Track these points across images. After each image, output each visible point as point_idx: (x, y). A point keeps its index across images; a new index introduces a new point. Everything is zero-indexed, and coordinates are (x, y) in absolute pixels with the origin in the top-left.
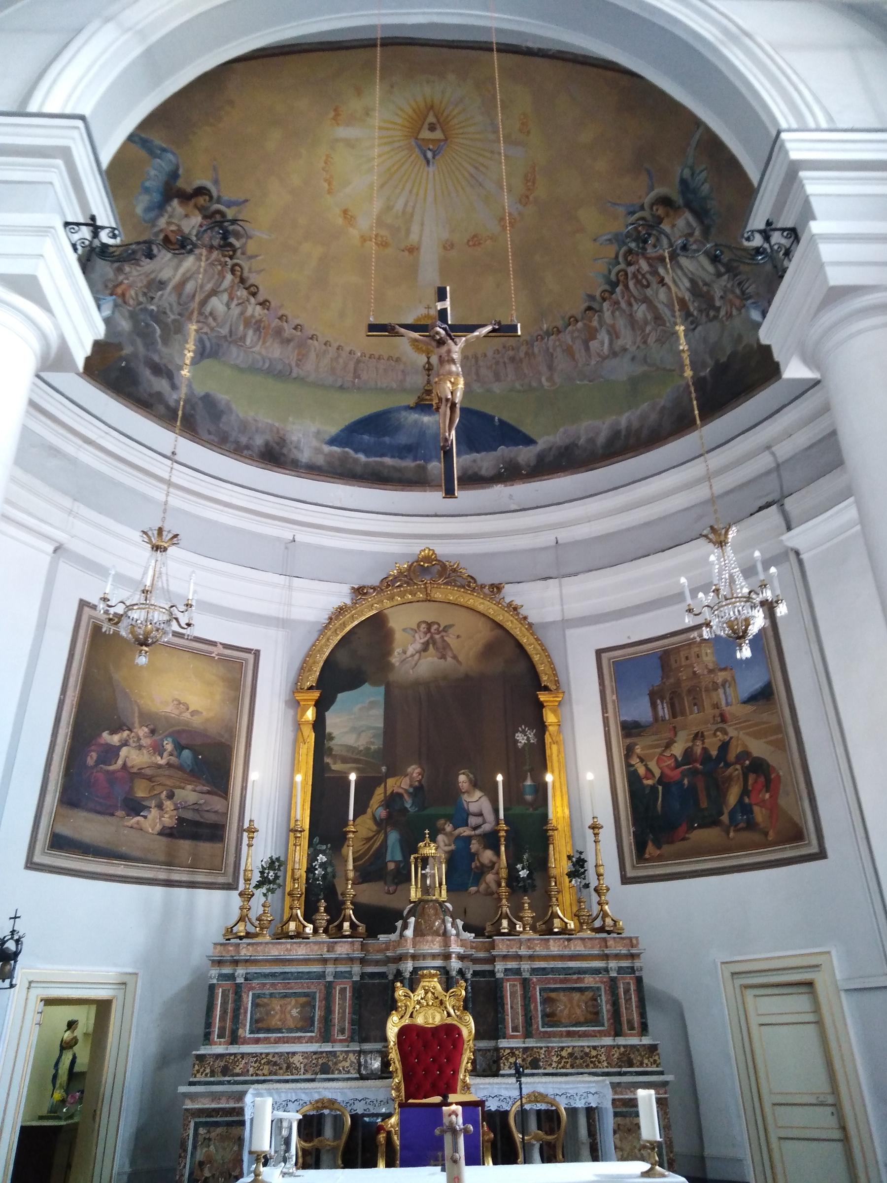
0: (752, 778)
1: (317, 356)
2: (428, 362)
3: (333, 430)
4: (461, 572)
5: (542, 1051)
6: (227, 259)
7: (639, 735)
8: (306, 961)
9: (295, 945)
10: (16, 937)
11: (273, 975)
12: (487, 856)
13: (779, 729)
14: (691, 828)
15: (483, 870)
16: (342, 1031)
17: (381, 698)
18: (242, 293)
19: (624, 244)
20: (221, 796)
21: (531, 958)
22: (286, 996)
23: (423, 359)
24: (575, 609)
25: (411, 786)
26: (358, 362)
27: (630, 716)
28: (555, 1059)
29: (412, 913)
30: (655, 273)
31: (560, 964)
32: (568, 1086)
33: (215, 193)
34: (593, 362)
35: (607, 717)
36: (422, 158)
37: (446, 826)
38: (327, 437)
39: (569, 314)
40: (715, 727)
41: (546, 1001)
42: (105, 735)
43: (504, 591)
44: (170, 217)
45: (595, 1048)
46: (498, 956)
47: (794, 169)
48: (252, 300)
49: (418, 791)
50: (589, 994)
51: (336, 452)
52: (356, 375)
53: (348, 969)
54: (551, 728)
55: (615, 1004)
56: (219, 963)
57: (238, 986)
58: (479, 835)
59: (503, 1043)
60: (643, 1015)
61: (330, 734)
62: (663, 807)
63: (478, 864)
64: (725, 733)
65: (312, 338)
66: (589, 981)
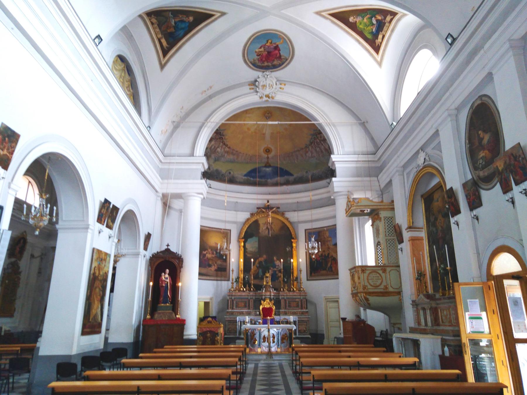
0: (333, 261)
3: (245, 173)
8: (245, 296)
12: (280, 274)
14: (321, 270)
17: (257, 240)
18: (224, 146)
21: (287, 296)
23: (266, 156)
24: (301, 219)
29: (264, 287)
38: (244, 175)
42: (203, 252)
47: (334, 162)
49: (265, 261)
55: (302, 304)
56: (229, 296)
59: (281, 310)
64: (329, 251)
66: (297, 300)
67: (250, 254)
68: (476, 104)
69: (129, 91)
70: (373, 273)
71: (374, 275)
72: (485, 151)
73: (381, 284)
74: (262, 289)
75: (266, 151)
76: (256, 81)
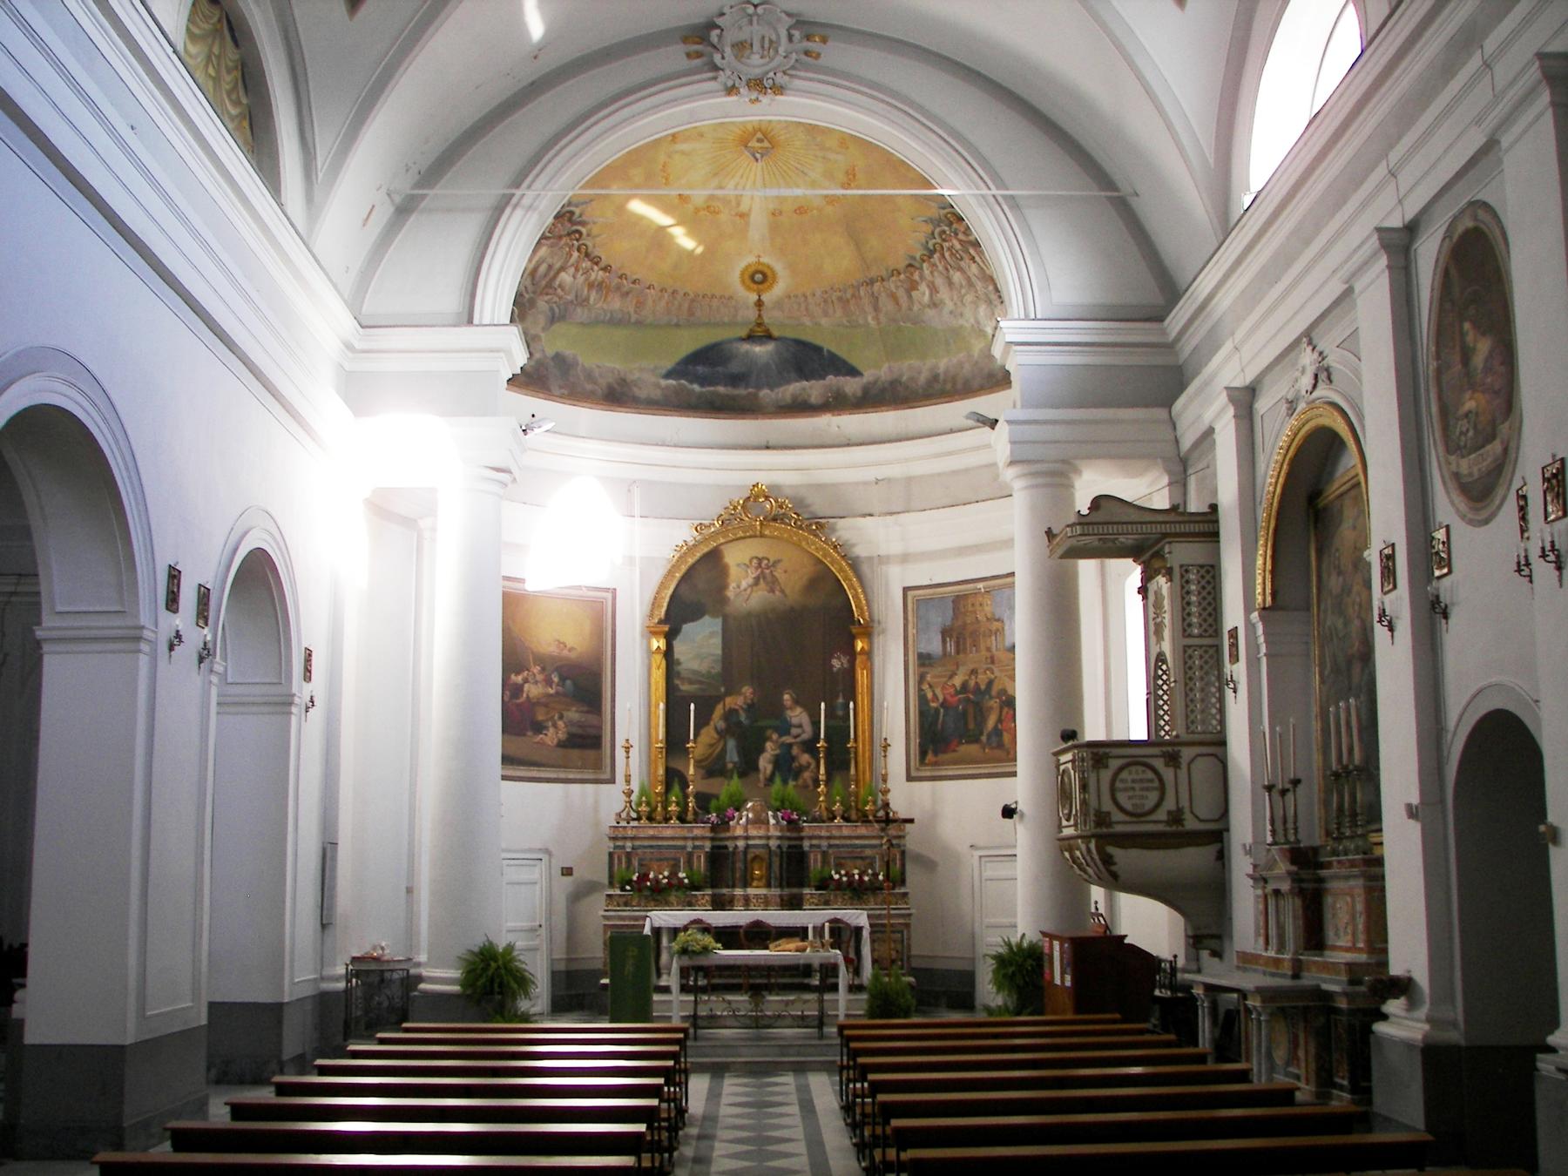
0: (1006, 710)
1: (654, 301)
2: (759, 300)
3: (668, 364)
6: (575, 242)
7: (931, 665)
8: (673, 838)
11: (651, 847)
12: (805, 758)
15: (801, 769)
18: (586, 264)
19: (939, 226)
21: (829, 838)
22: (661, 860)
23: (754, 297)
25: (745, 703)
27: (924, 649)
31: (848, 842)
32: (651, 832)
36: (752, 158)
38: (664, 371)
39: (891, 268)
40: (985, 666)
48: (596, 268)
49: (750, 707)
52: (691, 313)
61: (678, 660)
65: (649, 288)
66: (868, 852)
67: (691, 682)
68: (1460, 229)
69: (237, 103)
70: (1133, 769)
71: (1136, 773)
72: (1476, 395)
73: (1158, 805)
75: (752, 278)
76: (712, 25)
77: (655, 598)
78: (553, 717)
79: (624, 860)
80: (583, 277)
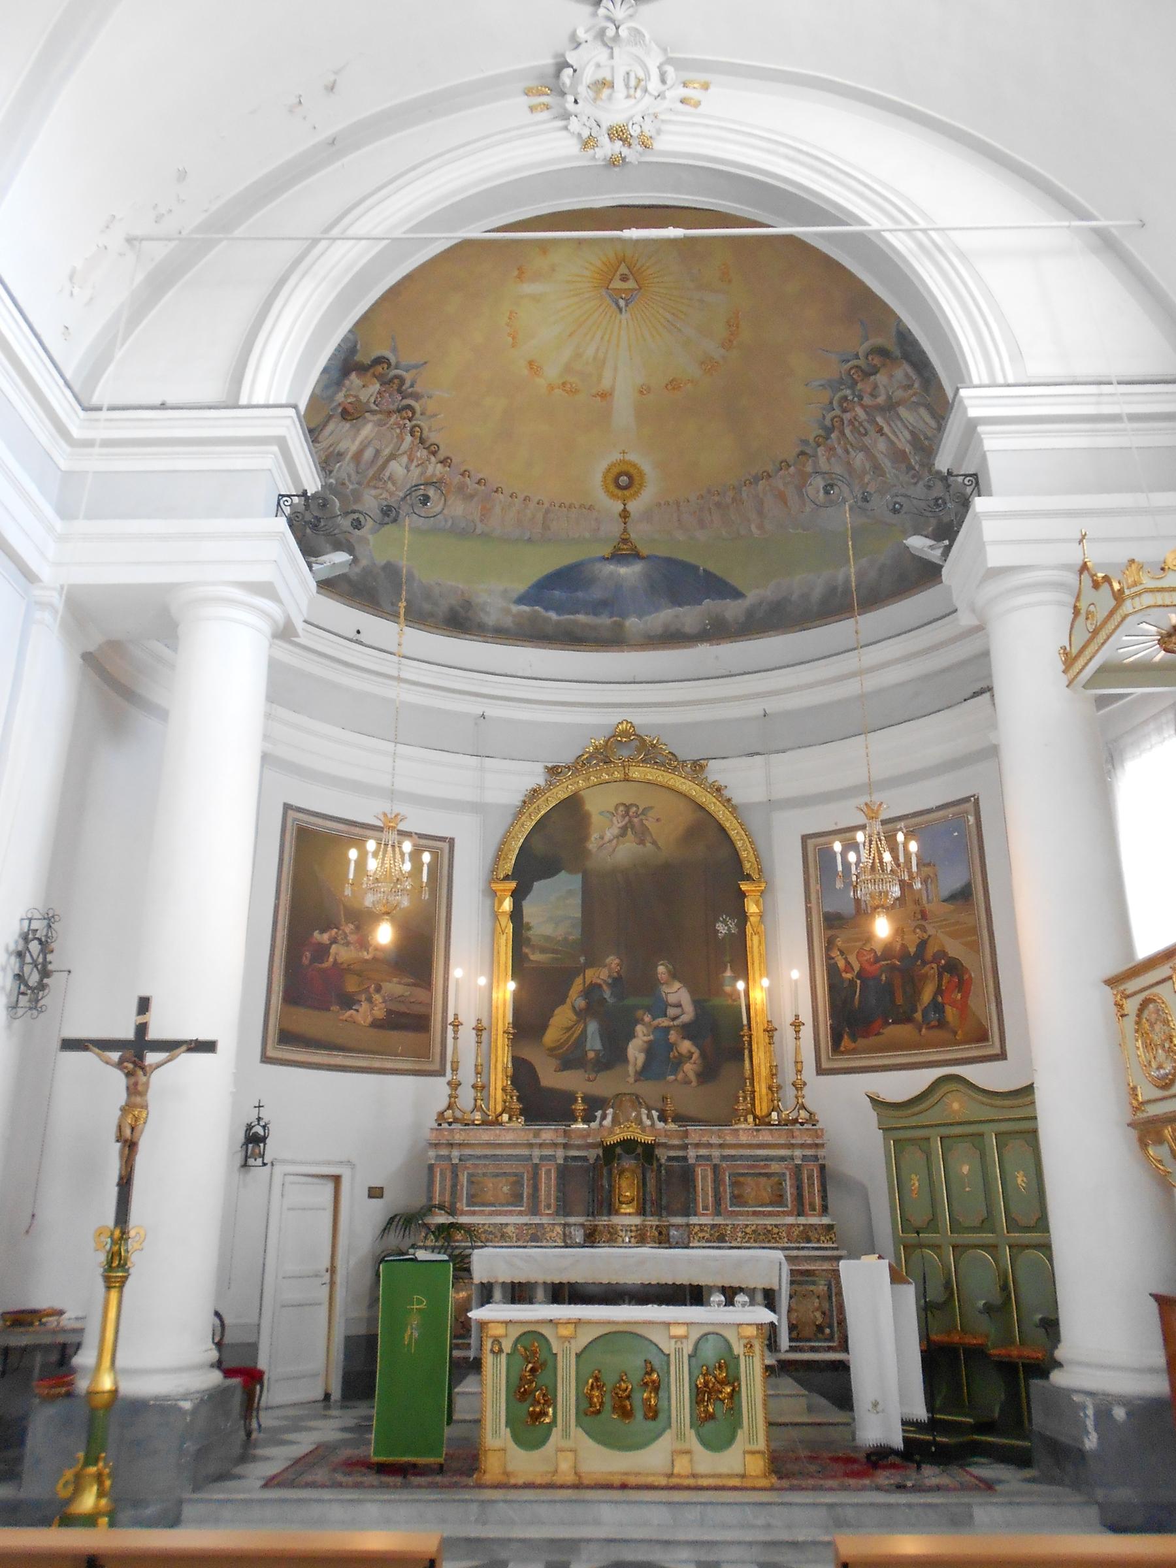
0: (946, 976)
1: (503, 509)
3: (521, 587)
4: (661, 748)
5: (729, 1228)
6: (407, 421)
7: (841, 927)
8: (514, 1145)
9: (503, 1131)
10: (262, 1123)
11: (486, 1157)
13: (974, 930)
15: (681, 1060)
16: (548, 1207)
18: (421, 453)
20: (426, 988)
21: (721, 1146)
22: (497, 1175)
24: (783, 791)
26: (547, 512)
28: (740, 1234)
30: (873, 421)
31: (748, 1152)
33: (393, 360)
34: (808, 509)
35: (810, 907)
36: (614, 306)
37: (645, 1016)
38: (515, 596)
41: (735, 1184)
42: (316, 934)
43: (707, 769)
44: (348, 390)
45: (776, 1226)
46: (691, 1144)
47: (972, 426)
48: (433, 459)
49: (616, 982)
50: (775, 1179)
51: (525, 612)
52: (546, 527)
53: (554, 1153)
54: (752, 919)
57: (455, 1166)
58: (678, 1026)
60: (824, 1198)
61: (528, 923)
62: (860, 1002)
63: (676, 1054)
64: (924, 929)
65: (496, 491)
66: (775, 1167)
67: (543, 950)
74: (599, 1114)
77: (500, 850)
78: (367, 989)
79: (448, 1174)
80: (419, 470)
